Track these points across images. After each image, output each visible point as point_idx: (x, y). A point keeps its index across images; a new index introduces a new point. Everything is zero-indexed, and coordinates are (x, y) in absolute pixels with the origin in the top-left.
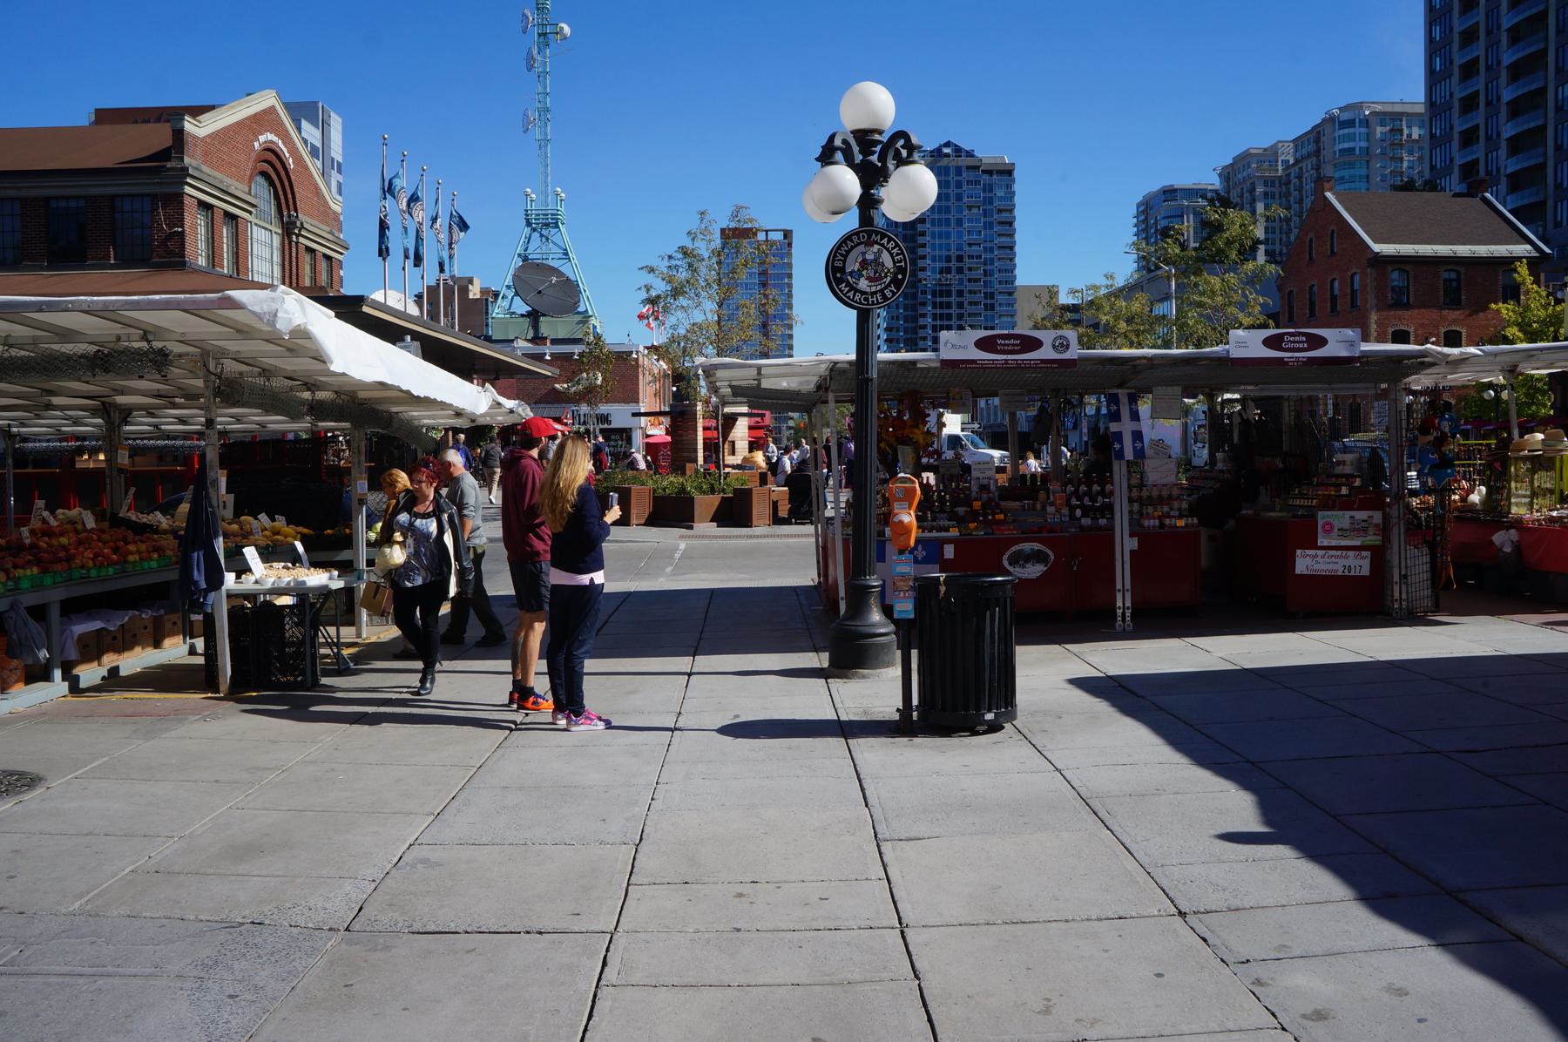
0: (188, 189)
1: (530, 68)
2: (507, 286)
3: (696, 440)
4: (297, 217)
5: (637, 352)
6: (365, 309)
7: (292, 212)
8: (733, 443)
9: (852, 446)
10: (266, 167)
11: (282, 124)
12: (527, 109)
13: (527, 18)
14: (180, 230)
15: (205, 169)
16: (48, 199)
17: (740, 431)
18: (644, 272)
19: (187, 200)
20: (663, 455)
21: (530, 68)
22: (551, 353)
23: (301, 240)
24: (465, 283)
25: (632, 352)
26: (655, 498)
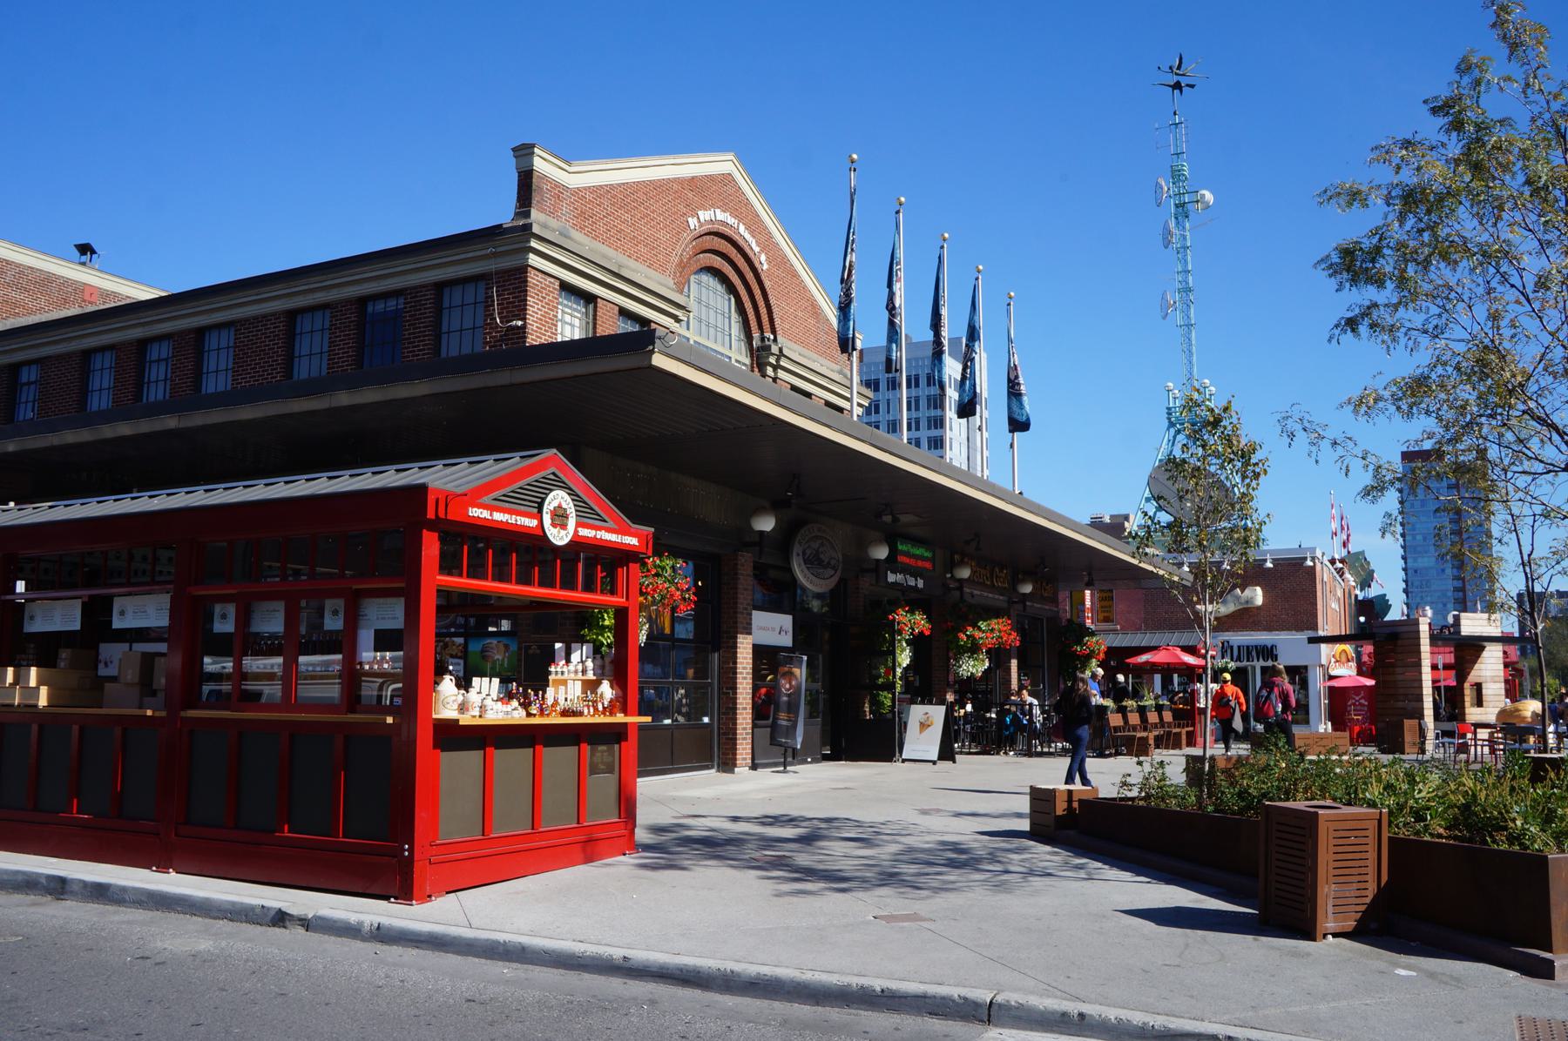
0: (533, 260)
1: (1167, 244)
2: (1146, 498)
3: (1421, 681)
4: (775, 340)
5: (1313, 559)
6: (659, 360)
7: (766, 335)
8: (1478, 687)
9: (668, 722)
10: (718, 262)
11: (748, 203)
12: (1165, 291)
13: (1162, 188)
14: (520, 323)
15: (577, 235)
16: (363, 301)
17: (1489, 667)
18: (1334, 210)
19: (533, 279)
20: (1354, 704)
21: (1167, 244)
22: (1190, 563)
23: (781, 374)
24: (1121, 520)
25: (1305, 559)
26: (1398, 847)
